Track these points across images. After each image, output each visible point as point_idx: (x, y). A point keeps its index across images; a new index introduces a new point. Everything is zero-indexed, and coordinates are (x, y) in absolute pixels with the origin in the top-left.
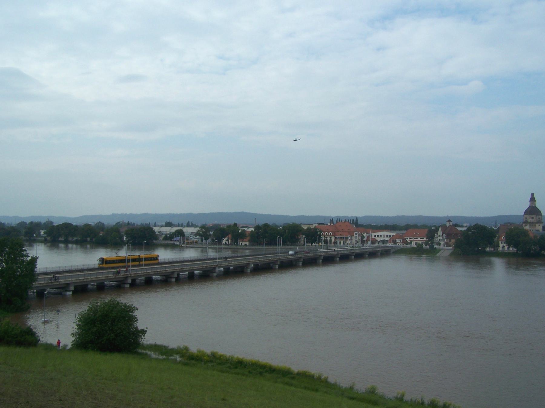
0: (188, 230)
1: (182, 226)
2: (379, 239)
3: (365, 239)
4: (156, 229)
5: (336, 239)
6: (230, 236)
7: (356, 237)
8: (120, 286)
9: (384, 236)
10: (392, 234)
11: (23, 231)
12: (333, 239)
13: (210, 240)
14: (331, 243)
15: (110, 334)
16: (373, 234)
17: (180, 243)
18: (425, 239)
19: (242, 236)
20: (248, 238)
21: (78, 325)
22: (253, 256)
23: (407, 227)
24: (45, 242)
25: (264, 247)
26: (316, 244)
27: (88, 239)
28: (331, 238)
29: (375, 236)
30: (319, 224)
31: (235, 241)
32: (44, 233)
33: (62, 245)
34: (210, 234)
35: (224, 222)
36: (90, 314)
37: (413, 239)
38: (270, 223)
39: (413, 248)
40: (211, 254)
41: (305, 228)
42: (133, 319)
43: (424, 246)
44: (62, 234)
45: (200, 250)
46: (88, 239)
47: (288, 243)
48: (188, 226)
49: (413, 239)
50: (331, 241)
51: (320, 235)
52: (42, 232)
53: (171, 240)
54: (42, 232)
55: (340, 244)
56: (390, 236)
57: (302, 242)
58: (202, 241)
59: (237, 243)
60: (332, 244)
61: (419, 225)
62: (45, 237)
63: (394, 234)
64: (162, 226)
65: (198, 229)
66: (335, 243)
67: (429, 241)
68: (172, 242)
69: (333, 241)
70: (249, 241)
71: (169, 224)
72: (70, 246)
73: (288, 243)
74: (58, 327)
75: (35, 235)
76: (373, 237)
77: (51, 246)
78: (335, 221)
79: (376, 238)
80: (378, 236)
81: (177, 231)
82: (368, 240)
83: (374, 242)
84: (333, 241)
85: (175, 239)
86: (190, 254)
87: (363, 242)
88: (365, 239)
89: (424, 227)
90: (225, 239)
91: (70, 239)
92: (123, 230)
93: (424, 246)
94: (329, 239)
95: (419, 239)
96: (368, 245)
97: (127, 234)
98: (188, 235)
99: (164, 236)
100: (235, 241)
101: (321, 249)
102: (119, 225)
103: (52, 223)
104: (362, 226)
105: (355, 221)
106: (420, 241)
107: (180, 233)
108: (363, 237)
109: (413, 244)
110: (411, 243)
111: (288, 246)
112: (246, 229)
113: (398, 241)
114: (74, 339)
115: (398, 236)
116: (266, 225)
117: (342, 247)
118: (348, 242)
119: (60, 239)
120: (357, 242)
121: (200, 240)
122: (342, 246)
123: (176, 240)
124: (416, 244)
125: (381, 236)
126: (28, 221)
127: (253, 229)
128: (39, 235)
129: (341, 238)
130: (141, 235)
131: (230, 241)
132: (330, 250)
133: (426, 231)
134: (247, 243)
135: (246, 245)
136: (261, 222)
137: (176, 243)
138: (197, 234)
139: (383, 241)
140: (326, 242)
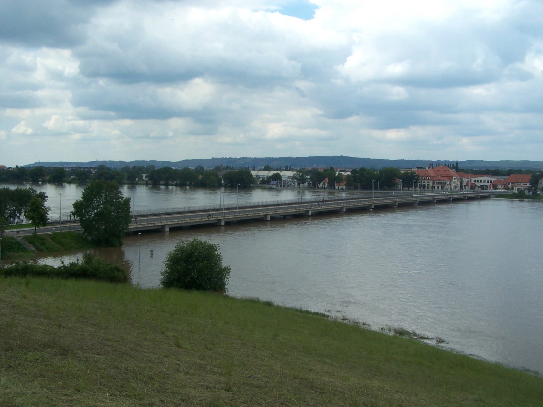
0: (286, 174)
1: (281, 170)
2: (479, 184)
3: (464, 184)
4: (254, 173)
5: (434, 183)
6: (327, 180)
7: (455, 182)
8: (211, 226)
9: (484, 181)
10: (493, 179)
11: (126, 175)
12: (431, 184)
13: (306, 184)
14: (428, 188)
15: (196, 273)
16: (473, 179)
17: (277, 186)
18: (528, 185)
19: (339, 179)
20: (345, 182)
21: (166, 264)
22: (348, 199)
23: (510, 172)
24: (147, 184)
25: (359, 191)
26: (413, 189)
27: (188, 182)
28: (428, 182)
29: (475, 181)
30: (418, 168)
31: (332, 185)
32: (146, 177)
33: (163, 187)
34: (307, 178)
35: (321, 168)
36: (177, 254)
37: (516, 184)
38: (368, 167)
39: (514, 193)
40: (308, 196)
41: (402, 172)
42: (218, 259)
43: (527, 192)
44: (161, 176)
45: (296, 192)
46: (188, 182)
47: (385, 187)
48: (286, 170)
49: (516, 184)
50: (428, 185)
51: (417, 179)
52: (144, 176)
53: (268, 184)
54: (144, 176)
55: (438, 189)
56: (491, 181)
57: (399, 187)
58: (299, 184)
59: (334, 187)
60: (430, 189)
61: (523, 170)
62: (146, 181)
63: (495, 179)
64: (261, 170)
65: (295, 172)
66: (433, 187)
67: (533, 186)
68: (269, 186)
69: (431, 185)
70: (345, 185)
71: (267, 168)
72: (170, 187)
73: (385, 187)
74: (148, 265)
75: (137, 179)
76: (472, 182)
77: (152, 188)
78: (434, 165)
79: (476, 183)
80: (478, 181)
81: (274, 175)
82: (467, 185)
83: (473, 187)
84: (431, 185)
85: (272, 183)
86: (287, 196)
87: (462, 187)
88: (464, 184)
89: (528, 172)
90: (322, 183)
91: (170, 182)
92: (221, 174)
93: (527, 192)
94: (426, 183)
95: (522, 184)
96: (467, 191)
97: (226, 177)
98: (285, 179)
99: (261, 179)
100: (332, 185)
101: (418, 195)
102: (218, 169)
103: (153, 167)
104: (462, 170)
105: (455, 165)
106: (522, 186)
107: (277, 177)
108: (462, 182)
109: (515, 191)
110: (513, 189)
111: (385, 190)
112: (343, 173)
113: (499, 186)
114: (162, 277)
115: (499, 182)
116: (363, 170)
117: (439, 193)
118: (446, 187)
119: (161, 183)
120: (456, 187)
121: (296, 184)
122: (439, 191)
123: (273, 183)
124: (518, 189)
125: (481, 181)
126: (131, 166)
127: (349, 173)
128: (141, 178)
129: (440, 183)
130: (236, 176)
131: (326, 185)
132: (428, 195)
133: (529, 177)
134: (344, 187)
135: (342, 189)
136: (358, 167)
137: (273, 187)
138: (294, 177)
139: (482, 187)
140: (424, 186)
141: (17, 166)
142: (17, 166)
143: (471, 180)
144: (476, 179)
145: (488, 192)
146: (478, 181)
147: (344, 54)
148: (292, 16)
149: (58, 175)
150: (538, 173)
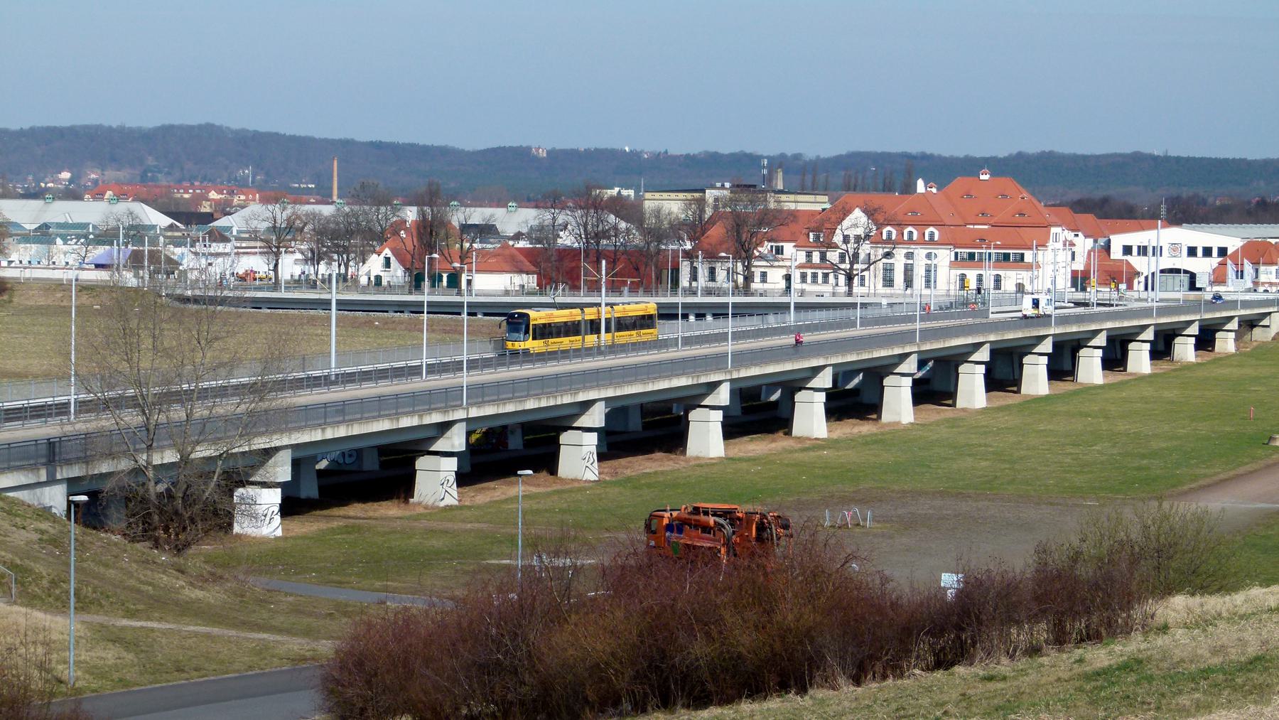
9: (1175, 247)
10: (1231, 238)
16: (1118, 241)
29: (1127, 250)
76: (1117, 253)
79: (1136, 261)
80: (1143, 251)
143: (1107, 248)
146: (1143, 251)
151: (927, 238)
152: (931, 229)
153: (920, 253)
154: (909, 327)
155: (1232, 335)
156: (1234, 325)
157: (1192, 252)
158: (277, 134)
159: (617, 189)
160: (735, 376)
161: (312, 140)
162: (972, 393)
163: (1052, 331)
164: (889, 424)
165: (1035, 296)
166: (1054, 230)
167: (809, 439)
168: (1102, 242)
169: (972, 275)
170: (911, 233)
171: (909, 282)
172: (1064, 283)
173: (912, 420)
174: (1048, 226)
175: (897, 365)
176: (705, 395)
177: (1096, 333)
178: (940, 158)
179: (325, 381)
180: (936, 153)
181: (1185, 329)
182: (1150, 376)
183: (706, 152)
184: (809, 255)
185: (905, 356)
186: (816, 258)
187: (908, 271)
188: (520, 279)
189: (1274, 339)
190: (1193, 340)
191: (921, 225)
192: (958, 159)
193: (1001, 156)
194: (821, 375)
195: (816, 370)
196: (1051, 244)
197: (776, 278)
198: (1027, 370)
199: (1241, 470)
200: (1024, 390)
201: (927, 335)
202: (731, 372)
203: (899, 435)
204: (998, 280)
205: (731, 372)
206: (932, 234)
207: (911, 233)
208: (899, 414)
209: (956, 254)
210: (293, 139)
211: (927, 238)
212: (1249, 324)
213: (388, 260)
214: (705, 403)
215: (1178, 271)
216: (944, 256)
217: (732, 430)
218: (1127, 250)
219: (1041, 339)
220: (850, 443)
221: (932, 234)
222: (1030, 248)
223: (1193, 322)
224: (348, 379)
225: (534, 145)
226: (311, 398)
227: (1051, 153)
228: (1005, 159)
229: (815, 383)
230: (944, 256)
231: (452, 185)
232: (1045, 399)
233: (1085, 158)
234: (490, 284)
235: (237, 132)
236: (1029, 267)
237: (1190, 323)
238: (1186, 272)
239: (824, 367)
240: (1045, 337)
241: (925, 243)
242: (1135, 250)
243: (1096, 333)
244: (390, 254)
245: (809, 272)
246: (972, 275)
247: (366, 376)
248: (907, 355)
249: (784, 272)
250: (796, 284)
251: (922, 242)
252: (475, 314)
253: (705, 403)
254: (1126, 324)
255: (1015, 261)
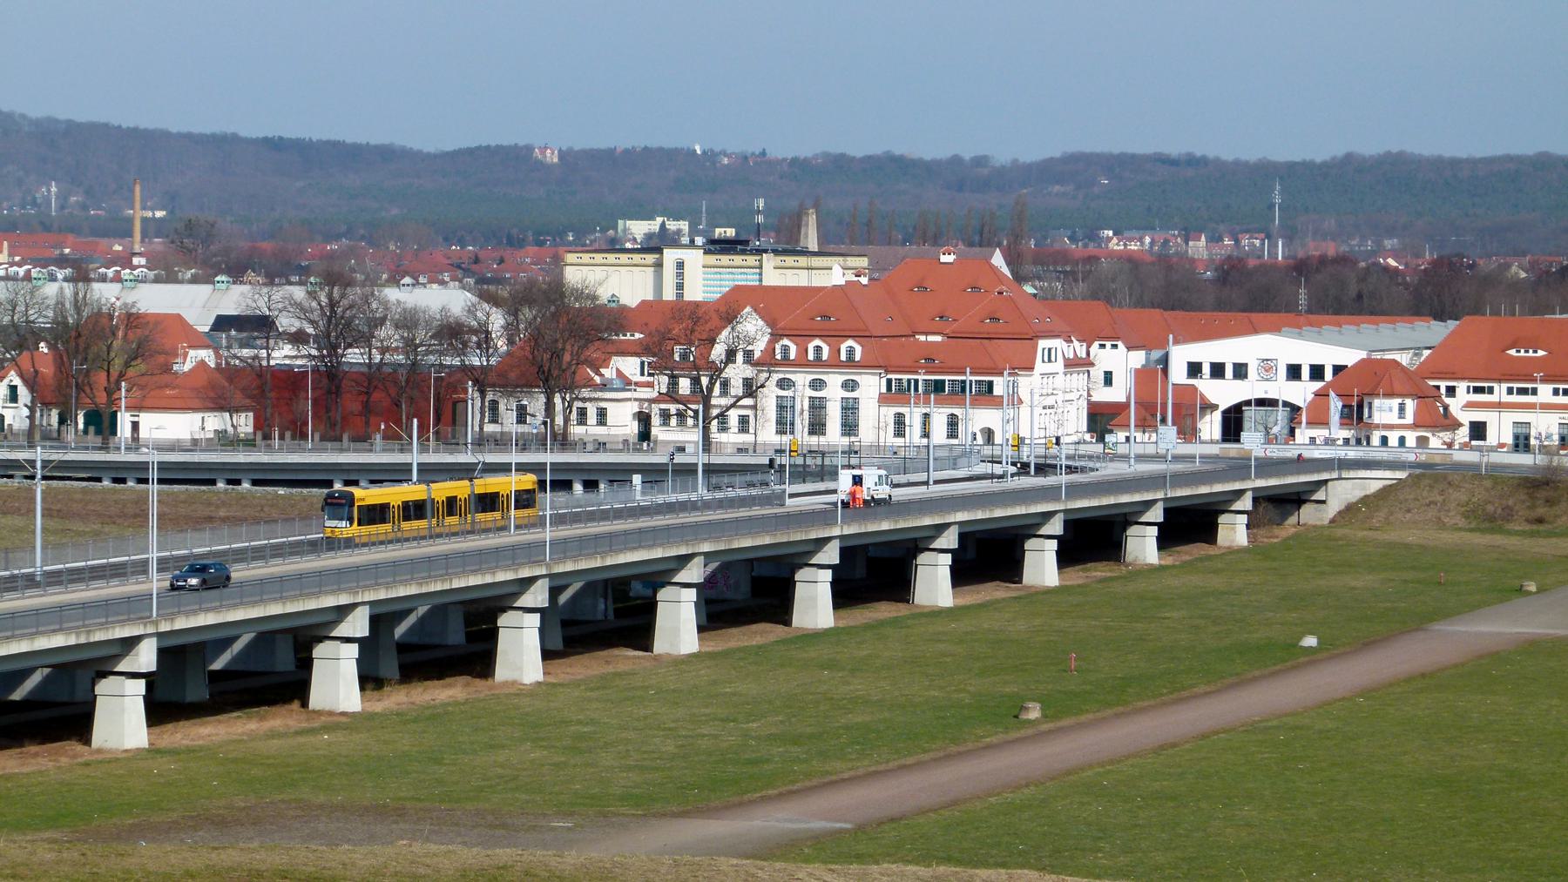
9: (1267, 365)
10: (1336, 350)
16: (1181, 355)
29: (1194, 369)
63: (1350, 357)
76: (1178, 374)
79: (1207, 387)
80: (1218, 370)
125: (1240, 371)
141: (763, 153)
142: (763, 153)
143: (1165, 361)
144: (1207, 352)
145: (1300, 463)
146: (1218, 370)
147: (543, 149)
148: (328, 142)
149: (424, 285)
150: (726, 161)
151: (843, 357)
152: (850, 342)
153: (834, 380)
154: (131, 587)
155: (1244, 519)
156: (1246, 503)
157: (1294, 372)
158: (106, 125)
159: (659, 220)
160: (165, 627)
161: (166, 135)
162: (676, 631)
163: (836, 532)
164: (505, 684)
165: (857, 472)
166: (1043, 344)
167: (331, 713)
168: (1157, 354)
169: (914, 415)
170: (818, 349)
171: (817, 427)
172: (1075, 424)
173: (539, 677)
174: (1034, 338)
175: (517, 595)
176: (118, 657)
177: (941, 528)
178: (1219, 164)
179: (30, 582)
180: (1211, 153)
181: (1142, 513)
182: (950, 609)
183: (826, 155)
184: (674, 383)
185: (529, 582)
186: (685, 385)
187: (817, 407)
188: (215, 422)
189: (1332, 521)
190: (1154, 531)
191: (833, 337)
192: (1246, 164)
193: (1318, 160)
194: (350, 618)
195: (343, 611)
196: (1040, 367)
197: (622, 419)
198: (800, 591)
199: (910, 761)
200: (797, 620)
201: (1074, 490)
202: (156, 623)
203: (525, 709)
204: (953, 423)
205: (156, 623)
206: (851, 351)
207: (818, 349)
208: (521, 669)
209: (889, 382)
210: (134, 133)
211: (843, 357)
212: (1283, 502)
213: (13, 389)
214: (120, 668)
215: (1272, 403)
216: (871, 385)
217: (159, 710)
218: (1194, 369)
219: (822, 542)
220: (400, 718)
221: (851, 351)
222: (1001, 374)
223: (1154, 502)
224: (54, 579)
225: (537, 142)
226: (433, 549)
227: (1401, 154)
228: (1324, 164)
229: (343, 630)
230: (871, 385)
231: (395, 211)
232: (826, 633)
233: (1455, 163)
234: (168, 430)
235: (37, 123)
236: (997, 403)
237: (1149, 504)
238: (1286, 404)
239: (354, 606)
240: (828, 540)
241: (808, 364)
242: (1206, 369)
243: (941, 528)
244: (17, 381)
245: (673, 408)
246: (914, 415)
247: (77, 576)
248: (531, 581)
249: (635, 407)
250: (657, 431)
251: (835, 364)
252: (123, 481)
253: (120, 668)
254: (1125, 499)
255: (953, 393)
